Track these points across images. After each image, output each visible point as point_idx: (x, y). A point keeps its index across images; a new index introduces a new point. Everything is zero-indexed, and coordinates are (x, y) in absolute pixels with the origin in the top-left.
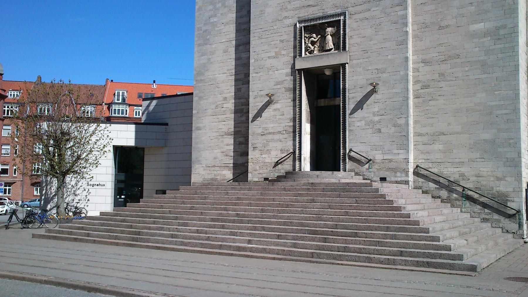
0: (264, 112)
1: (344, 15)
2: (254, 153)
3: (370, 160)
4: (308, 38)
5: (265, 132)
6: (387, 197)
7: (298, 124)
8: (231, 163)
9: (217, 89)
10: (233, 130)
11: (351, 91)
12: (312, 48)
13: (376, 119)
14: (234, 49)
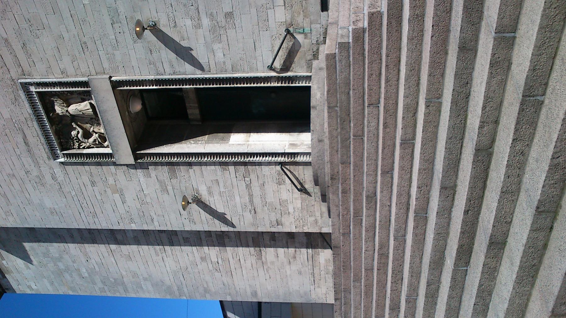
0: (215, 209)
1: (26, 86)
2: (287, 224)
3: (288, 31)
4: (81, 143)
5: (251, 208)
6: (360, 25)
7: (230, 159)
8: (306, 252)
9: (189, 269)
10: (253, 248)
11: (159, 70)
12: (95, 136)
13: (206, 21)
14: (123, 247)
